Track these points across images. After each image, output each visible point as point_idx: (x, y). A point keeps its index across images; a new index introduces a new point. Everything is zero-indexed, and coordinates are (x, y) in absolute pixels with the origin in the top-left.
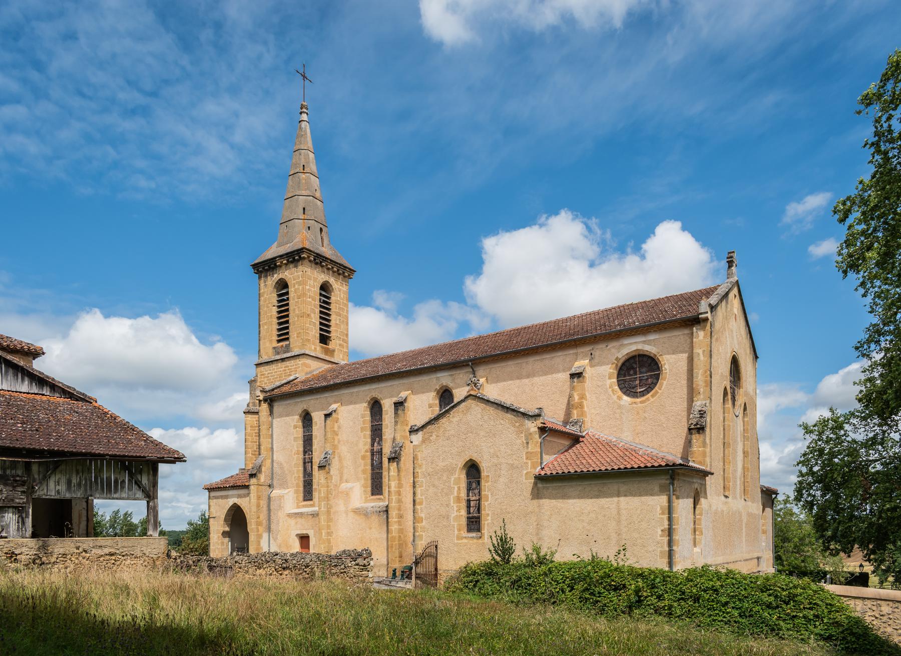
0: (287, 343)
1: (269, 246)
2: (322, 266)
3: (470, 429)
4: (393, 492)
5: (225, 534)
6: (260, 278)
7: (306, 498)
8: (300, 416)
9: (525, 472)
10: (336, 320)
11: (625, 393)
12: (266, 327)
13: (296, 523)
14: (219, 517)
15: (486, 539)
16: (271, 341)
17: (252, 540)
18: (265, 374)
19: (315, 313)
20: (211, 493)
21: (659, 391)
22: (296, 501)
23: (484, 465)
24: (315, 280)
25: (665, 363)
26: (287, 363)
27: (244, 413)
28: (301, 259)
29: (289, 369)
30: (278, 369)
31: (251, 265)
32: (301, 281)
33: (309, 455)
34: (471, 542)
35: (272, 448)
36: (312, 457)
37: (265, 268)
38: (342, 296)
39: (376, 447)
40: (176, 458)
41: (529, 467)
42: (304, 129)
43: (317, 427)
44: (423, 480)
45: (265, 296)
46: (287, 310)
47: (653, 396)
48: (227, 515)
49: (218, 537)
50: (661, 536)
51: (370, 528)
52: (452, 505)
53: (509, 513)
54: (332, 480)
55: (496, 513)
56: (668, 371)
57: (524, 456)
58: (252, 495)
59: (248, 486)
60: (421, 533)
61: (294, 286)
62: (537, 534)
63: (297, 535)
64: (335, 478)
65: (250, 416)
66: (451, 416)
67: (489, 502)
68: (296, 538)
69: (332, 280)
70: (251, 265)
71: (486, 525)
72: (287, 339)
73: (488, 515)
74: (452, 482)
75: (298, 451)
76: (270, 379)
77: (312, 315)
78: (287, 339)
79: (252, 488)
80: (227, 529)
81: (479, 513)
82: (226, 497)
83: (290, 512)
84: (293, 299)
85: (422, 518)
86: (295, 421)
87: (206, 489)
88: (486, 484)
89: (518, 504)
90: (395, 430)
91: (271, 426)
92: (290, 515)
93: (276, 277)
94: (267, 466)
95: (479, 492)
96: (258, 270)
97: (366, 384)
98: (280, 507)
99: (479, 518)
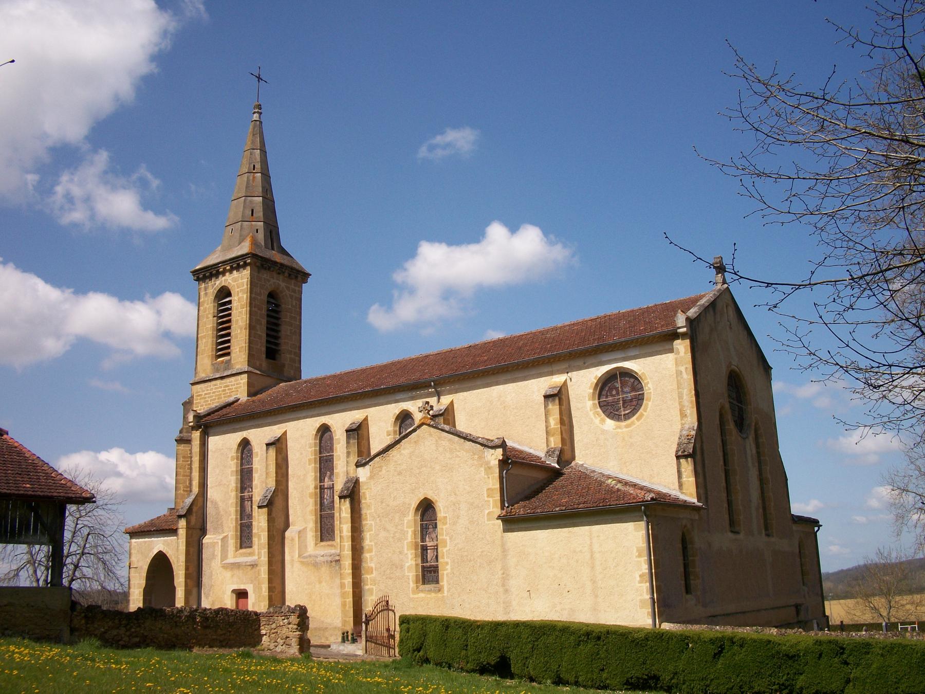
0: (229, 357)
1: (211, 251)
3: (423, 463)
4: (345, 538)
9: (487, 512)
11: (608, 416)
13: (232, 576)
14: (141, 568)
15: (446, 592)
17: (180, 596)
18: (201, 395)
19: (261, 324)
21: (645, 413)
23: (440, 505)
25: (648, 383)
26: (227, 380)
27: (176, 440)
29: (228, 389)
31: (191, 272)
33: (249, 492)
34: (429, 596)
36: (252, 495)
37: (206, 274)
39: (327, 483)
40: (85, 499)
41: (491, 505)
43: (258, 458)
44: (373, 523)
45: (206, 305)
46: (229, 321)
47: (638, 419)
50: (640, 582)
51: (320, 582)
52: (406, 552)
53: (470, 561)
55: (456, 561)
56: (651, 391)
57: (485, 492)
60: (372, 587)
61: (238, 295)
62: (503, 585)
63: (234, 591)
66: (402, 447)
67: (448, 548)
70: (191, 272)
71: (445, 576)
73: (447, 563)
74: (405, 524)
76: (207, 401)
78: (228, 354)
81: (437, 562)
84: (237, 309)
85: (372, 568)
88: (444, 527)
89: (481, 550)
90: (347, 462)
95: (437, 536)
97: (315, 407)
99: (437, 567)
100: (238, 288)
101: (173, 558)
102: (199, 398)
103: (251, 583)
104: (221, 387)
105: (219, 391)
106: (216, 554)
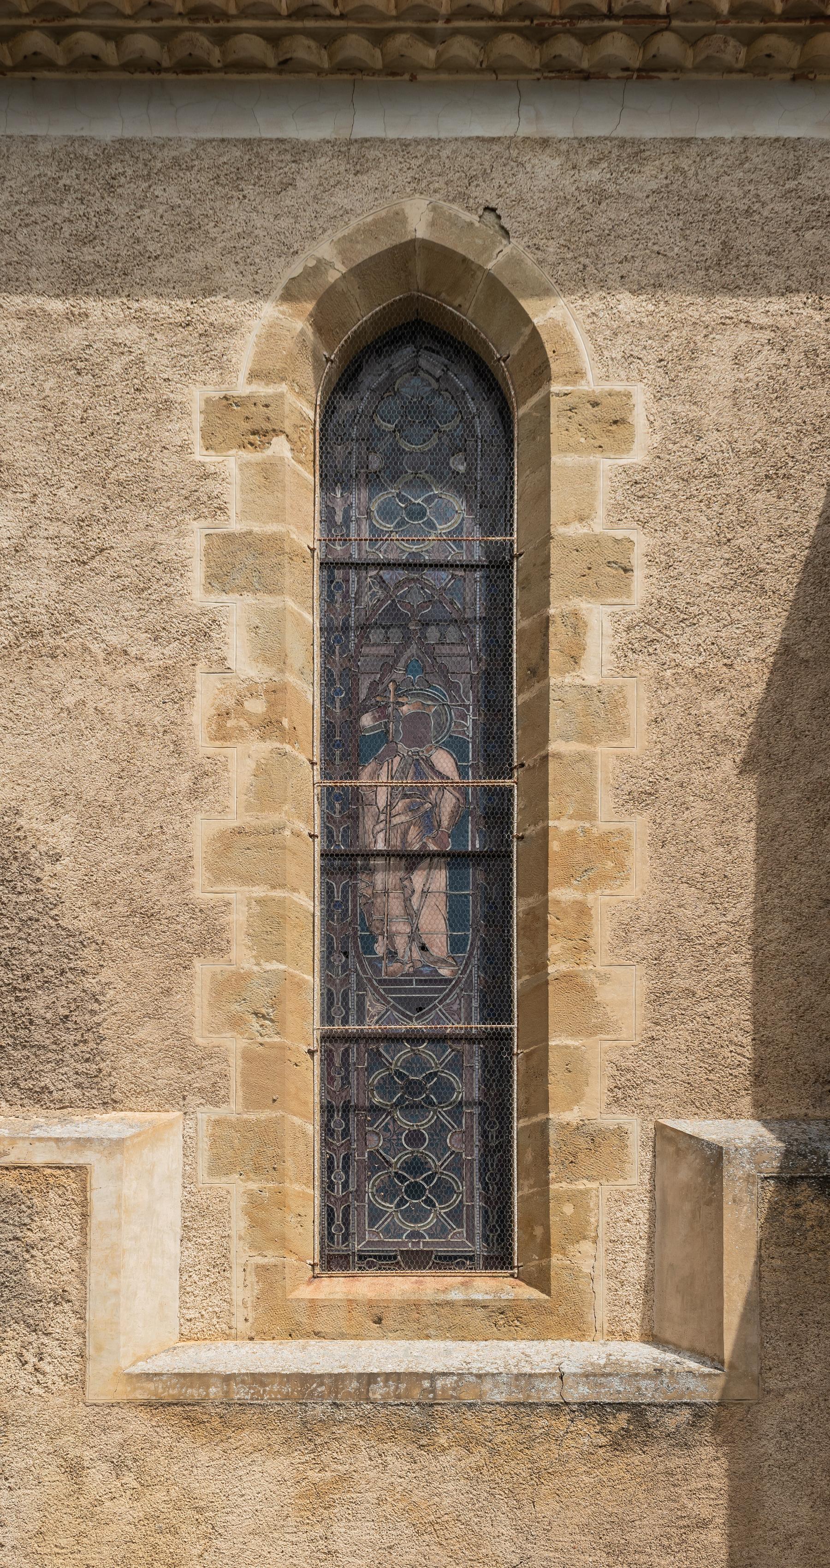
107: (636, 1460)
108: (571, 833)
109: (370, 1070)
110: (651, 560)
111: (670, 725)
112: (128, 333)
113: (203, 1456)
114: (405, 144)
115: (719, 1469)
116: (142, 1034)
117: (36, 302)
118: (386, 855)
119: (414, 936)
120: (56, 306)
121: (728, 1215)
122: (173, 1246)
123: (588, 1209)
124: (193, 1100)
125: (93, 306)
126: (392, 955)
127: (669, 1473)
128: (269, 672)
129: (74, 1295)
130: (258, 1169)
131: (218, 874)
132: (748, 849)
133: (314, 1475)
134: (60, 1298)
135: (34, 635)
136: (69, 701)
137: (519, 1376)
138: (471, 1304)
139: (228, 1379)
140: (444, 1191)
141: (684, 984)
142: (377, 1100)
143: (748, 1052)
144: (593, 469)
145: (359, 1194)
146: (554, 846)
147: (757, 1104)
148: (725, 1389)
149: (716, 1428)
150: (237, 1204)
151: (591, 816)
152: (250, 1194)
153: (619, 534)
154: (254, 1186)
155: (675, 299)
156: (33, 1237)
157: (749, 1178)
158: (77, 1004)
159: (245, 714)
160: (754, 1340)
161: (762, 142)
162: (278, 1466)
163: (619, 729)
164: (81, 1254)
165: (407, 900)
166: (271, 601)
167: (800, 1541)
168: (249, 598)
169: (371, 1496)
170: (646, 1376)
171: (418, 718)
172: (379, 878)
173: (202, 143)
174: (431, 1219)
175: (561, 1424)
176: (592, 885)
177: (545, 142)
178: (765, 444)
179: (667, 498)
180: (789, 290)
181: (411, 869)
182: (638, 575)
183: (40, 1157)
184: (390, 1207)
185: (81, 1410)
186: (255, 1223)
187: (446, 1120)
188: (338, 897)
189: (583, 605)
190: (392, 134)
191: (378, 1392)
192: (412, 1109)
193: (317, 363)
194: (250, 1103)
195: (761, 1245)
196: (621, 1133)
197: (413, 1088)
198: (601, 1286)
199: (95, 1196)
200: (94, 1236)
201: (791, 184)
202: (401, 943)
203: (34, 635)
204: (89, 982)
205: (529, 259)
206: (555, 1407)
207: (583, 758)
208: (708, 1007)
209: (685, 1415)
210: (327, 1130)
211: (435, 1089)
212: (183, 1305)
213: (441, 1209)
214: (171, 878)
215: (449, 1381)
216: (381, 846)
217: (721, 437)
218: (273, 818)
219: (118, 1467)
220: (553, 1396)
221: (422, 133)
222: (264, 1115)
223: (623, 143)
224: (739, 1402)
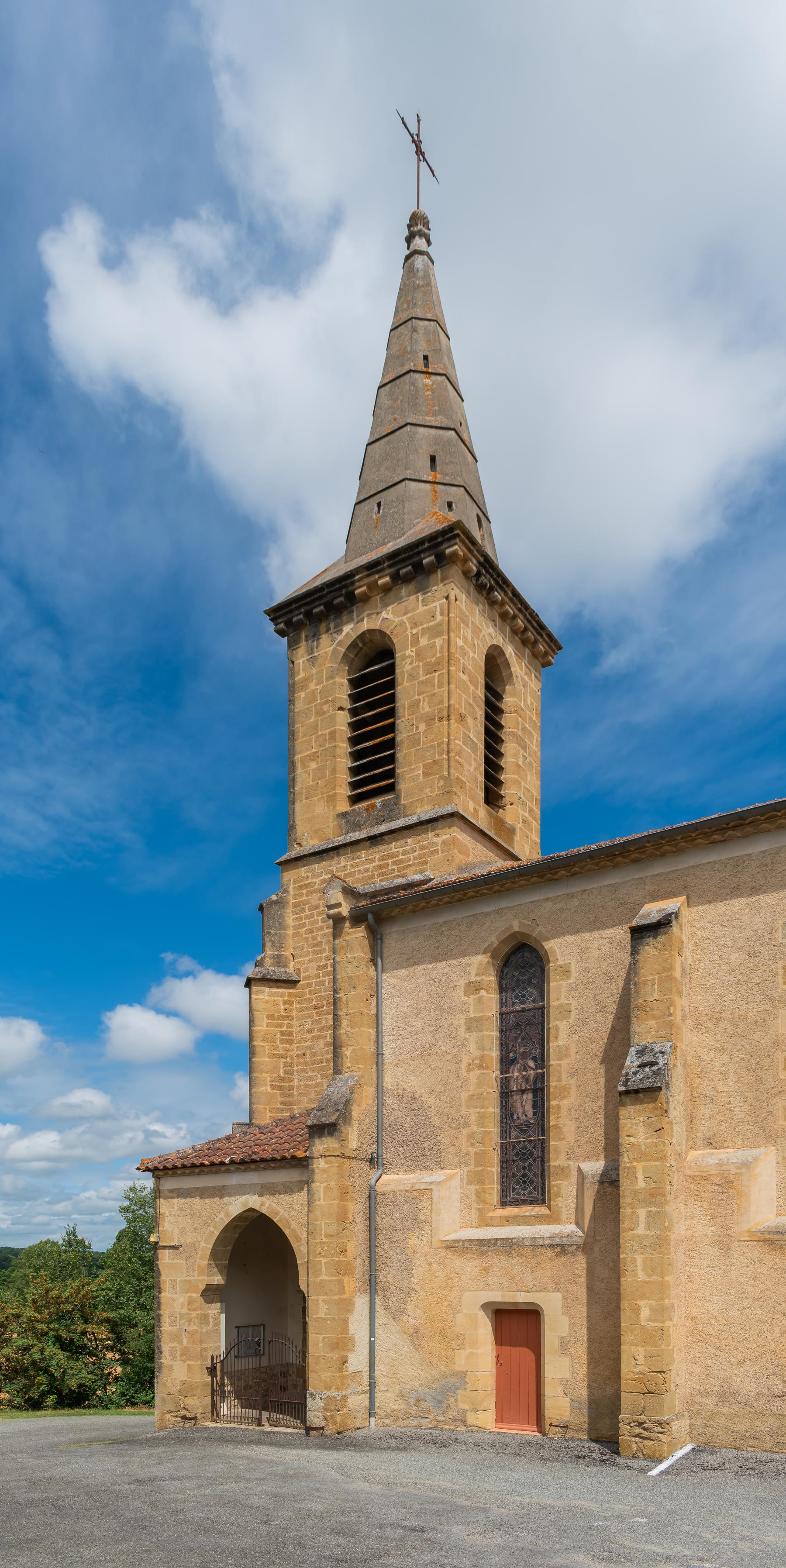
0: (390, 796)
2: (492, 603)
5: (210, 1293)
6: (293, 645)
7: (540, 1197)
8: (493, 957)
10: (516, 756)
12: (313, 765)
13: (485, 1271)
14: (193, 1247)
16: (331, 799)
20: (162, 1182)
22: (475, 1206)
24: (477, 631)
26: (393, 847)
28: (442, 560)
29: (395, 863)
30: (358, 865)
32: (440, 624)
35: (379, 1054)
38: (529, 702)
42: (421, 274)
45: (312, 686)
48: (220, 1241)
49: (191, 1301)
54: (672, 1137)
58: (319, 1187)
59: (306, 1159)
61: (416, 639)
63: (485, 1306)
64: (678, 1133)
65: (267, 989)
68: (481, 1314)
69: (510, 651)
72: (391, 788)
75: (482, 1057)
77: (470, 721)
78: (391, 788)
79: (320, 1165)
80: (218, 1279)
82: (221, 1192)
83: (447, 1238)
86: (473, 970)
87: (148, 1170)
91: (376, 992)
92: (456, 1247)
93: (349, 631)
94: (364, 1105)
96: (288, 623)
98: (416, 1222)
100: (415, 625)
101: (294, 1225)
102: (305, 891)
103: (556, 1290)
104: (372, 861)
105: (367, 870)
106: (422, 1217)
107: (562, 1259)
108: (556, 1086)
109: (513, 1150)
110: (576, 1008)
111: (581, 1053)
112: (446, 970)
113: (458, 1260)
114: (512, 907)
115: (584, 1261)
116: (450, 1150)
117: (426, 966)
118: (516, 1091)
119: (524, 1112)
120: (430, 966)
121: (586, 1193)
122: (457, 1205)
123: (560, 1188)
124: (463, 1166)
125: (438, 964)
126: (518, 1118)
127: (571, 1263)
128: (480, 1052)
129: (429, 1221)
130: (478, 1183)
131: (468, 1106)
132: (603, 1085)
133: (484, 1265)
134: (426, 1222)
135: (425, 1051)
136: (433, 1066)
137: (533, 1238)
138: (531, 1216)
139: (464, 1241)
140: (532, 1182)
141: (585, 1124)
142: (514, 1158)
143: (603, 1142)
144: (561, 985)
145: (510, 1184)
146: (551, 1090)
147: (606, 1157)
148: (585, 1240)
149: (583, 1250)
150: (473, 1192)
151: (561, 1081)
152: (476, 1189)
153: (567, 1002)
154: (477, 1187)
155: (582, 935)
156: (420, 1207)
157: (591, 1183)
158: (435, 1144)
159: (474, 1064)
160: (593, 1226)
161: (605, 886)
162: (476, 1262)
163: (568, 1056)
164: (431, 1211)
165: (522, 1103)
166: (480, 1034)
167: (605, 1280)
168: (475, 1034)
169: (497, 1270)
170: (564, 1237)
171: (524, 1052)
172: (515, 1097)
173: (463, 918)
174: (528, 1190)
175: (543, 1250)
176: (561, 1099)
177: (547, 899)
178: (606, 970)
179: (581, 990)
180: (613, 926)
181: (523, 1094)
182: (573, 1013)
183: (422, 1187)
184: (518, 1187)
185: (431, 1250)
186: (478, 1197)
187: (533, 1163)
188: (504, 1104)
189: (558, 1023)
190: (509, 905)
191: (499, 1243)
192: (524, 1160)
193: (494, 965)
194: (476, 1166)
195: (595, 1200)
196: (569, 1167)
197: (524, 1154)
198: (564, 1210)
199: (434, 1196)
200: (434, 1206)
201: (614, 896)
202: (520, 1115)
203: (425, 1051)
204: (438, 1138)
205: (544, 931)
206: (542, 1246)
207: (559, 1065)
208: (592, 1130)
209: (575, 1247)
210: (502, 1167)
211: (529, 1154)
212: (461, 1219)
213: (531, 1187)
214: (457, 1109)
215: (516, 1240)
216: (515, 1089)
217: (595, 971)
218: (482, 1090)
219: (439, 1263)
220: (541, 1243)
221: (517, 903)
222: (479, 1169)
223: (568, 895)
224: (588, 1243)
